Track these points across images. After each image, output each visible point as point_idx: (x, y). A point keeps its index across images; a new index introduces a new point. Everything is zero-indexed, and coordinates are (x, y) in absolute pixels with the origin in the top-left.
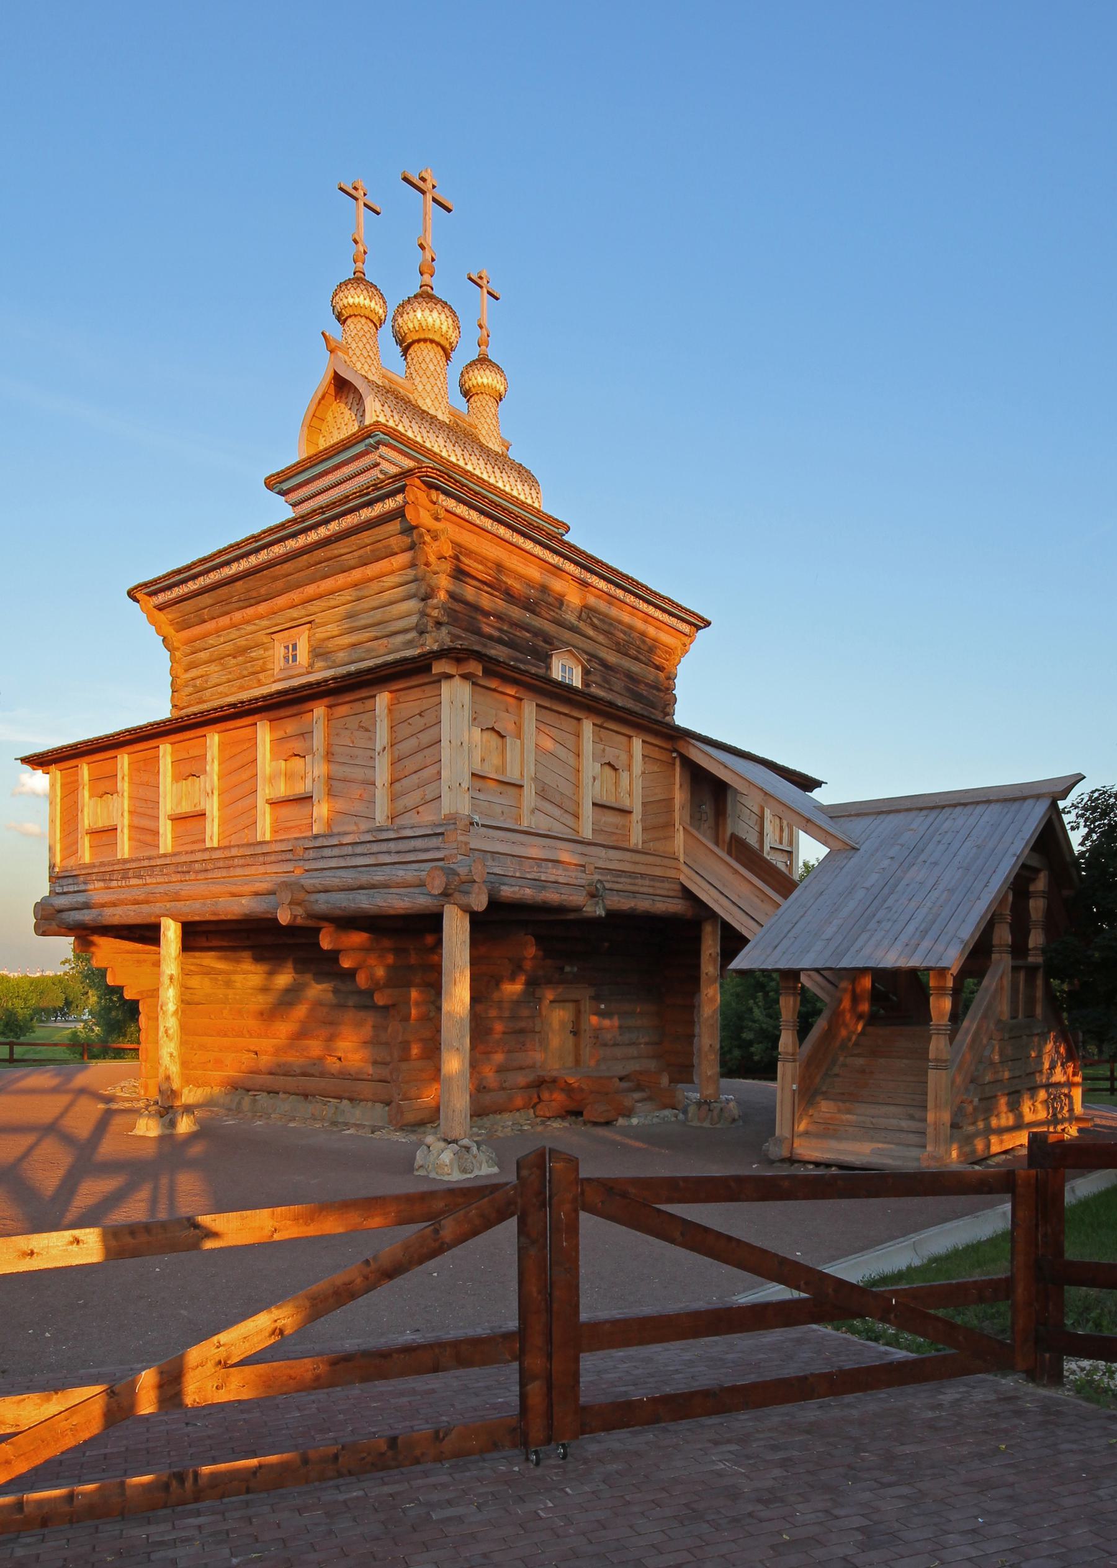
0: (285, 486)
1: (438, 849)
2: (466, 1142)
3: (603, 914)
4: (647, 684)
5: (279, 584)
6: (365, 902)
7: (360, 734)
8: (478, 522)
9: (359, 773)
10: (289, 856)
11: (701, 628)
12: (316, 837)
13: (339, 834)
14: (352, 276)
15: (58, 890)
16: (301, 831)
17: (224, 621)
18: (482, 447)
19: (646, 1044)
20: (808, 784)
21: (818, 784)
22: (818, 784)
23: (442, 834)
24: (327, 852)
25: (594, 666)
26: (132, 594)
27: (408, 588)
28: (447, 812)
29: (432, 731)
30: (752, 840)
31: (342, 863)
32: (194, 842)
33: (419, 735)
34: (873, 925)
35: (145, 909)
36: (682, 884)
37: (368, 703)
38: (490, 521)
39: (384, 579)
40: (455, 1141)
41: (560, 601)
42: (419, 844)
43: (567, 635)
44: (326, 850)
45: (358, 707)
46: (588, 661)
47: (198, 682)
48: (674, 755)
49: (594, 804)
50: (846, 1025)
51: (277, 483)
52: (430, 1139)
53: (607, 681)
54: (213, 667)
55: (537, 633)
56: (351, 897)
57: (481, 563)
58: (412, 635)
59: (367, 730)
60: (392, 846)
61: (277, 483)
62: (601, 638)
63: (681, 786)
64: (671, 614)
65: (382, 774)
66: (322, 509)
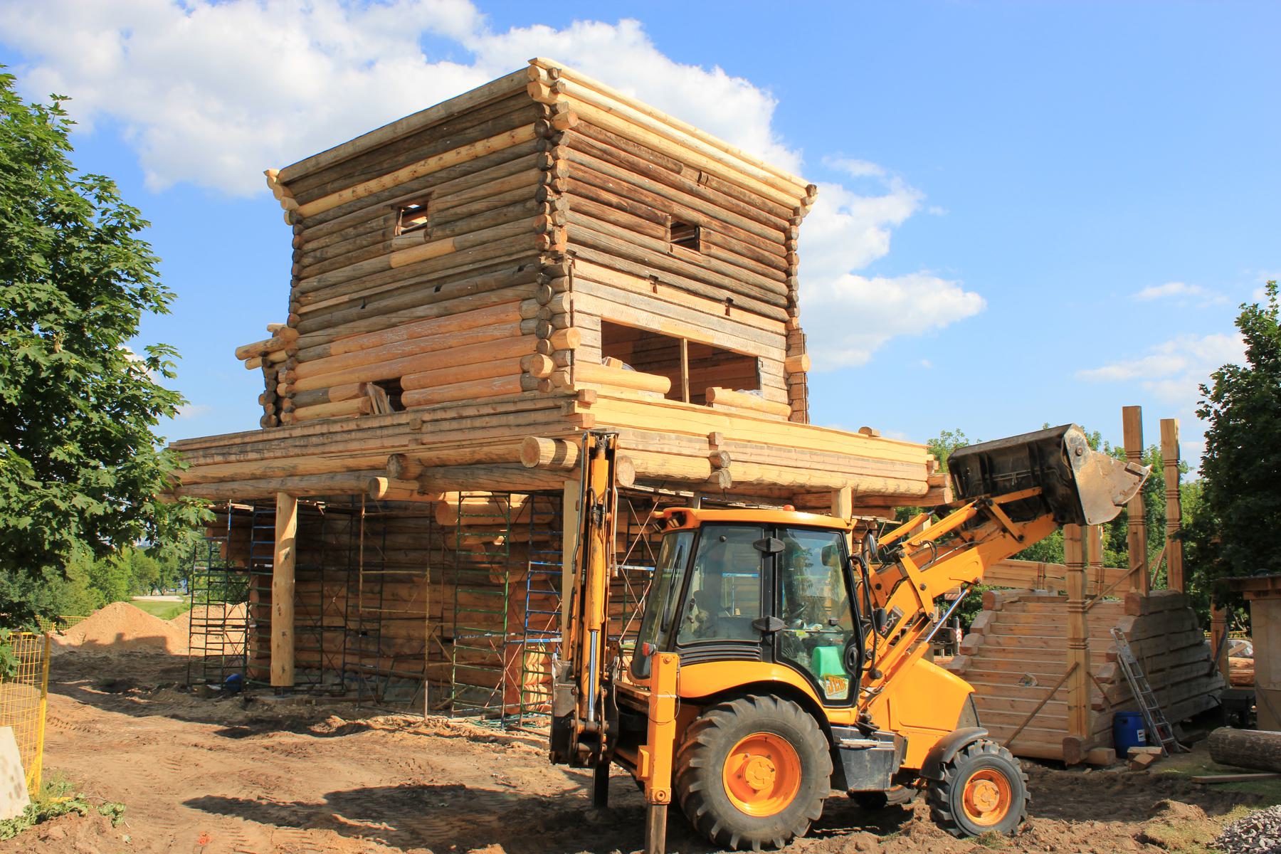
24: (446, 426)
26: (1125, 409)
47: (318, 254)
54: (335, 238)
58: (532, 204)
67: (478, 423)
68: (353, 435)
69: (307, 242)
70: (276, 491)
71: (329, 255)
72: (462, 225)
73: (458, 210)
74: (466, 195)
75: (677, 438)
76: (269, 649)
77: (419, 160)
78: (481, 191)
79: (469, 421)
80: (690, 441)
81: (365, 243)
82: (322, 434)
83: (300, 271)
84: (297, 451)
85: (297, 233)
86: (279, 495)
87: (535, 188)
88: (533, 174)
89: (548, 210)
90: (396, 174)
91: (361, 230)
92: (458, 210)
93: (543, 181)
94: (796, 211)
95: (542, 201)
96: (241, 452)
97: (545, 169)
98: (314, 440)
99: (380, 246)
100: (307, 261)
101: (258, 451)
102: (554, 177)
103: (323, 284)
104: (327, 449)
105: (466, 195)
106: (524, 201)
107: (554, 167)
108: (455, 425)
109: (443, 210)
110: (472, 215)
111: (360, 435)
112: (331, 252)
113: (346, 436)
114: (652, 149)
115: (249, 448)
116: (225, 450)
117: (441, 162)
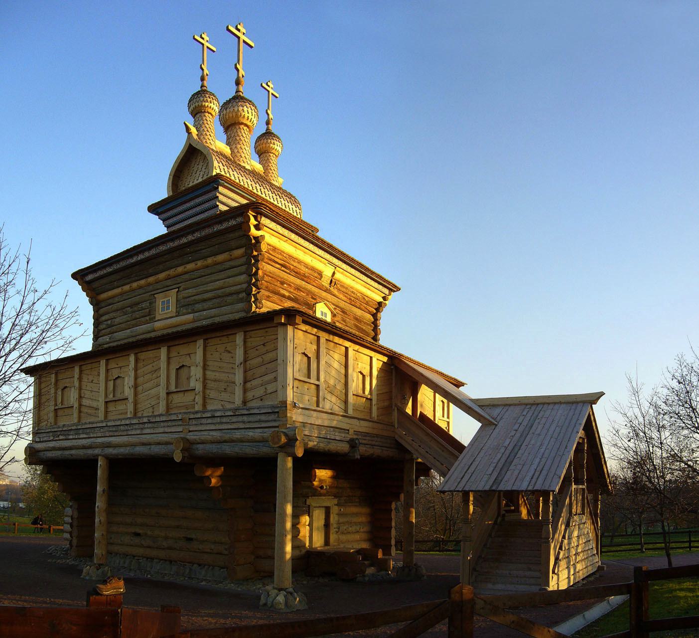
0: (160, 210)
1: (275, 421)
2: (291, 590)
3: (359, 457)
4: (365, 323)
5: (161, 267)
6: (227, 449)
7: (226, 354)
8: (281, 232)
9: (223, 376)
10: (180, 423)
11: (394, 291)
12: (197, 412)
13: (211, 411)
14: (200, 89)
15: (38, 440)
16: (187, 408)
17: (126, 288)
18: (271, 185)
19: (364, 532)
20: (458, 384)
21: (462, 384)
22: (462, 384)
23: (278, 412)
25: (339, 311)
26: (75, 276)
27: (196, 268)
28: (281, 400)
29: (274, 353)
30: (431, 417)
31: (213, 427)
32: (119, 414)
33: (263, 356)
34: (512, 467)
35: (90, 452)
36: (396, 441)
37: (231, 337)
38: (287, 231)
39: (225, 263)
40: (284, 590)
41: (320, 274)
42: (263, 418)
43: (324, 294)
44: (203, 420)
45: (225, 339)
46: (335, 309)
47: (109, 322)
48: (392, 367)
49: (353, 395)
50: (213, 472)
51: (154, 209)
52: (269, 588)
53: (344, 321)
54: (118, 313)
55: (309, 292)
56: (219, 446)
57: (281, 254)
58: (244, 294)
59: (229, 352)
60: (245, 418)
61: (154, 209)
62: (341, 296)
63: (396, 384)
64: (379, 283)
65: (239, 378)
66: (197, 223)
67: (224, 420)
68: (146, 425)
69: (102, 316)
70: (98, 455)
71: (116, 323)
72: (198, 306)
73: (196, 297)
74: (202, 288)
75: (334, 431)
76: (274, 552)
77: (172, 268)
78: (211, 286)
79: (218, 419)
80: (340, 432)
81: (138, 316)
82: (127, 425)
83: (99, 331)
84: (111, 434)
85: (96, 311)
86: (100, 458)
87: (245, 286)
88: (243, 278)
89: (253, 299)
90: (157, 276)
91: (136, 308)
92: (196, 297)
93: (249, 283)
94: (380, 304)
95: (249, 294)
96: (76, 434)
97: (251, 276)
98: (122, 427)
99: (148, 318)
100: (102, 327)
101: (86, 434)
102: (257, 280)
103: (112, 340)
104: (130, 433)
105: (202, 288)
106: (238, 293)
107: (256, 273)
108: (210, 421)
109: (186, 298)
110: (205, 300)
111: (150, 425)
112: (117, 320)
113: (141, 426)
114: (306, 266)
115: (81, 431)
116: (67, 433)
117: (185, 270)
